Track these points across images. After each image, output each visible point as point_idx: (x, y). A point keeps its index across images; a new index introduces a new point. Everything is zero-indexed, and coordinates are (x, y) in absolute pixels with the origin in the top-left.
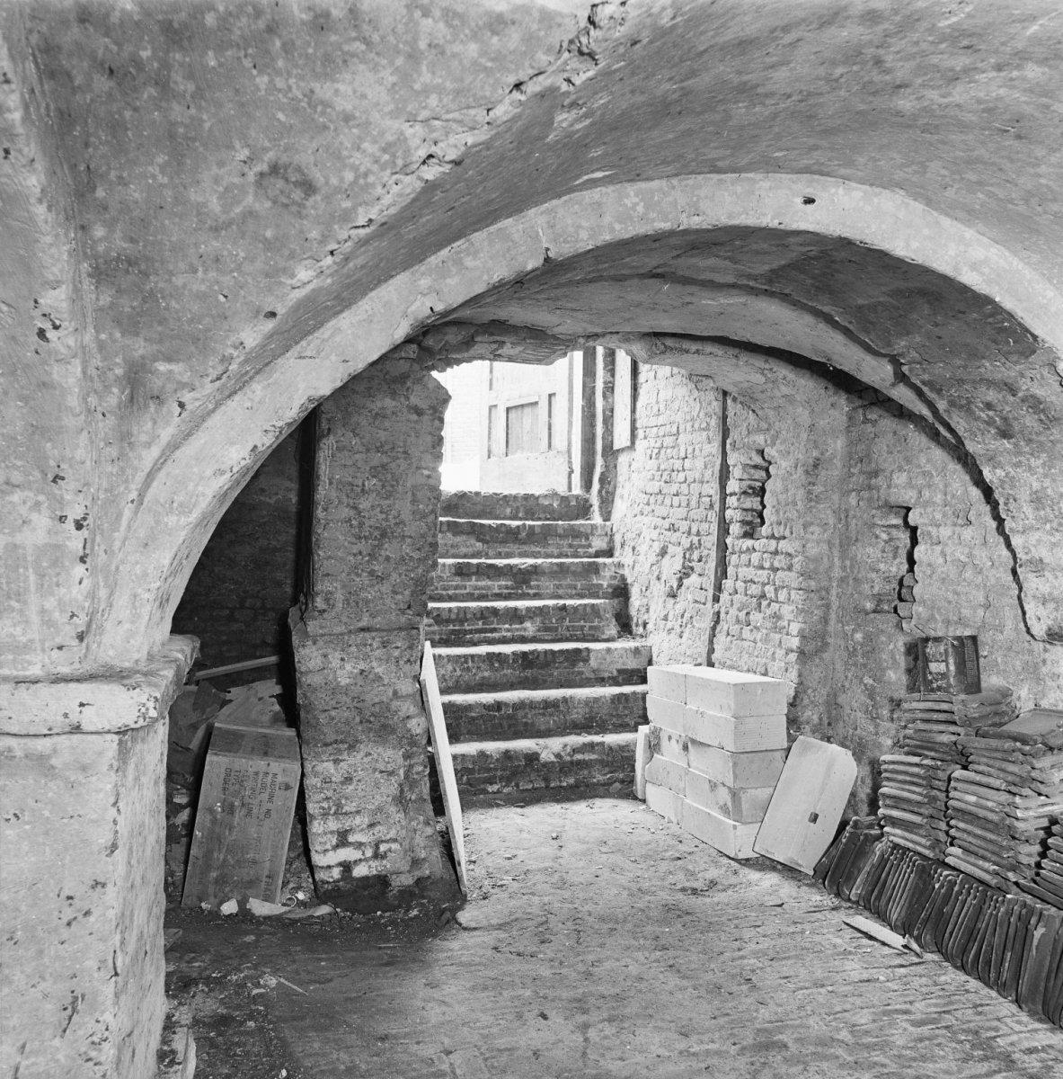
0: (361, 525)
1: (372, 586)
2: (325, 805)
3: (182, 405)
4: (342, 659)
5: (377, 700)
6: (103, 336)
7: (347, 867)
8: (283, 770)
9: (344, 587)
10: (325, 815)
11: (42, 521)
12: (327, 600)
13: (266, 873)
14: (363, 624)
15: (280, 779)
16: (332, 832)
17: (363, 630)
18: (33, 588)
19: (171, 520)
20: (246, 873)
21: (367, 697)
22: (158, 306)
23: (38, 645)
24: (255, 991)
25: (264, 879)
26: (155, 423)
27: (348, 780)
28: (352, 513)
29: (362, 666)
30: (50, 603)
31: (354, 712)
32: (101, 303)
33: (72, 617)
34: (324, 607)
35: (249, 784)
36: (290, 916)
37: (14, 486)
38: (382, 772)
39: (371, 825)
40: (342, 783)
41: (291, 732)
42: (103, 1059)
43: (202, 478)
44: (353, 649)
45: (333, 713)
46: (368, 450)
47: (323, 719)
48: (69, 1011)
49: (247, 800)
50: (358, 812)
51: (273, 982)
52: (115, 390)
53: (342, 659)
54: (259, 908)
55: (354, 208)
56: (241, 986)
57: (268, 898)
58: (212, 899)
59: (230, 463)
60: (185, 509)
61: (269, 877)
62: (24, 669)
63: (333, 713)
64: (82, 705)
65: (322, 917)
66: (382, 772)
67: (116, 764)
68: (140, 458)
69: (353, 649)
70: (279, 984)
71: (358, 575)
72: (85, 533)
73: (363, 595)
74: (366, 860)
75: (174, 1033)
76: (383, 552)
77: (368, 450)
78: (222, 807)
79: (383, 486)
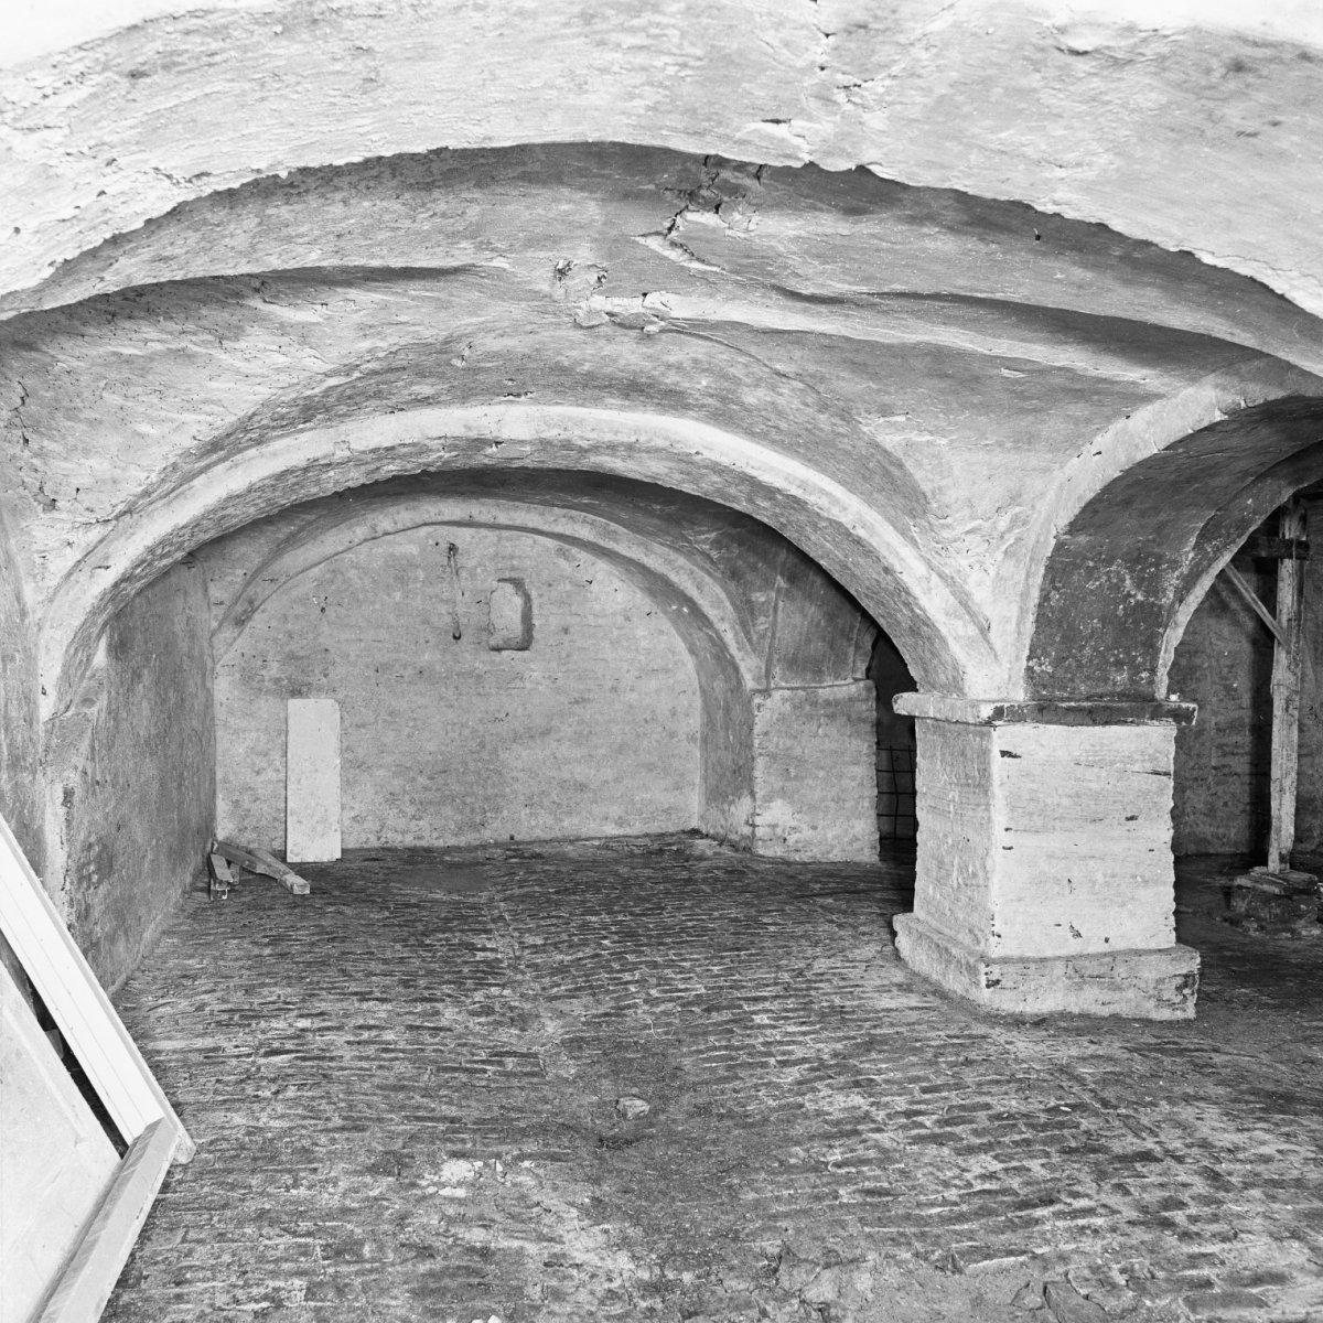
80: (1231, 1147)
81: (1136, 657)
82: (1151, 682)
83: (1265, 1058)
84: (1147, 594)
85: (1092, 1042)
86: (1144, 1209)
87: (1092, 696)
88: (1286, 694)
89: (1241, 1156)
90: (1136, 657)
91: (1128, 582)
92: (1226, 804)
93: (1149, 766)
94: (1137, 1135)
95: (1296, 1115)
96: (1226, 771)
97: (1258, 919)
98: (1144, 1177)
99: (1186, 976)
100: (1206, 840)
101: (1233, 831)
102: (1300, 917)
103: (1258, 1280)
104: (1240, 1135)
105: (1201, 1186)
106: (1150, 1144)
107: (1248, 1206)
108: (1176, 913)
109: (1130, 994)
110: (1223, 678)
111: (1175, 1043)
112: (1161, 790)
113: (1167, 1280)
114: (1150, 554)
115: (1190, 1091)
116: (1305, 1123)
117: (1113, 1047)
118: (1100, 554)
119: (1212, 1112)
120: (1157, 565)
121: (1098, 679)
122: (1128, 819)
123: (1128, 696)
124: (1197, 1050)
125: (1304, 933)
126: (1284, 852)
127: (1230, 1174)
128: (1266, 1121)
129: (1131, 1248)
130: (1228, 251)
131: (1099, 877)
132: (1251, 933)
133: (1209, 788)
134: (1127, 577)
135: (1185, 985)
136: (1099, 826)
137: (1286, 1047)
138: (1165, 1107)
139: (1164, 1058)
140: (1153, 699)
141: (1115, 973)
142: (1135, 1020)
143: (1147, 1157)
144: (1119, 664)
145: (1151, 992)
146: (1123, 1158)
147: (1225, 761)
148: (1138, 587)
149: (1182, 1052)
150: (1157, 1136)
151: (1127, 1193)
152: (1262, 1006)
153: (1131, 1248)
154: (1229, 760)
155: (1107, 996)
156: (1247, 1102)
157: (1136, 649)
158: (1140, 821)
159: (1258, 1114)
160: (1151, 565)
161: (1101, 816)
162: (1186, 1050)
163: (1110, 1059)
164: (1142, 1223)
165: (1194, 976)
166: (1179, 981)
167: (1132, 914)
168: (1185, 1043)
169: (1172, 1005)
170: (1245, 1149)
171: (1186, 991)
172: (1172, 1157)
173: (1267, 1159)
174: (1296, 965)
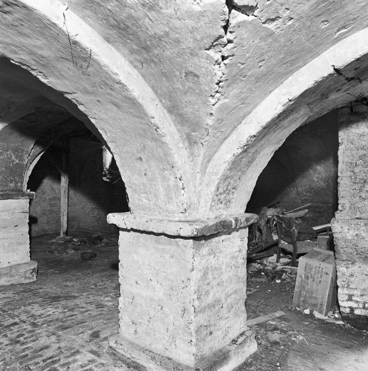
0: (356, 178)
1: (361, 202)
2: (343, 283)
3: (202, 144)
4: (349, 229)
5: (363, 246)
6: (178, 128)
7: (352, 309)
8: (328, 267)
9: (349, 202)
10: (343, 287)
11: (172, 178)
12: (343, 207)
13: (320, 303)
14: (358, 216)
15: (324, 270)
16: (346, 294)
17: (358, 219)
18: (174, 196)
19: (213, 177)
20: (313, 301)
21: (359, 245)
22: (184, 117)
23: (176, 212)
24: (293, 339)
25: (319, 305)
26: (198, 149)
27: (352, 275)
28: (352, 174)
29: (357, 232)
30: (178, 201)
31: (354, 250)
32: (173, 119)
33: (183, 204)
34: (342, 209)
35: (313, 270)
36: (327, 321)
37: (165, 170)
38: (366, 275)
39: (362, 295)
40: (350, 276)
41: (332, 253)
42: (191, 328)
43: (221, 165)
44: (353, 226)
45: (345, 249)
46: (358, 149)
47: (341, 251)
48: (183, 312)
49: (313, 276)
50: (356, 289)
51: (301, 338)
52: (186, 142)
53: (349, 229)
54: (317, 315)
55: (212, 79)
56: (290, 336)
57: (321, 312)
58: (301, 307)
59: (227, 160)
60: (217, 174)
61: (321, 304)
62: (175, 218)
63: (345, 249)
64: (180, 228)
65: (339, 325)
66: (366, 275)
67: (192, 246)
68: (197, 160)
69: (353, 226)
70: (303, 340)
71: (354, 197)
72: (182, 181)
73: (357, 205)
74: (360, 308)
75: (242, 336)
76: (365, 189)
77: (358, 149)
78: (305, 276)
79: (365, 163)
80: (40, 314)
81: (17, 179)
82: (21, 186)
83: (54, 288)
84: (20, 160)
85: (3, 294)
86: (11, 340)
87: (3, 191)
88: (64, 189)
89: (42, 316)
90: (17, 179)
91: (13, 157)
92: (52, 220)
93: (21, 211)
94: (13, 318)
95: (59, 301)
96: (52, 211)
97: (58, 250)
98: (13, 330)
99: (33, 269)
100: (47, 230)
101: (54, 227)
102: (68, 248)
103: (41, 349)
104: (43, 311)
105: (30, 328)
106: (17, 320)
107: (42, 331)
108: (30, 252)
109: (17, 277)
110: (50, 186)
111: (29, 289)
112: (25, 217)
113: (15, 359)
114: (19, 149)
115: (31, 302)
116: (61, 303)
117: (10, 294)
118: (4, 148)
119: (36, 306)
120: (22, 153)
121: (5, 186)
122: (15, 226)
123: (14, 190)
124: (35, 290)
125: (69, 252)
126: (64, 231)
127: (38, 322)
128: (51, 305)
129: (5, 353)
130: (18, 60)
131: (6, 244)
132: (56, 254)
133: (47, 216)
134: (13, 155)
135: (33, 272)
136: (6, 229)
137: (60, 284)
138: (23, 308)
139: (25, 294)
140: (22, 191)
141: (12, 272)
142: (18, 284)
143: (15, 324)
144: (11, 181)
145: (23, 275)
146: (6, 327)
147: (51, 208)
148: (17, 159)
149: (30, 291)
150: (19, 317)
151: (7, 336)
152: (55, 274)
153: (5, 353)
154: (53, 208)
155: (9, 279)
156: (47, 301)
157: (16, 177)
158: (19, 226)
159: (49, 304)
160: (20, 152)
161: (6, 226)
162: (32, 290)
163: (8, 298)
164: (10, 344)
165: (35, 269)
166: (31, 271)
167: (17, 254)
168: (32, 288)
169: (29, 278)
170: (44, 314)
171: (33, 273)
172: (23, 322)
173: (49, 315)
174: (66, 261)
